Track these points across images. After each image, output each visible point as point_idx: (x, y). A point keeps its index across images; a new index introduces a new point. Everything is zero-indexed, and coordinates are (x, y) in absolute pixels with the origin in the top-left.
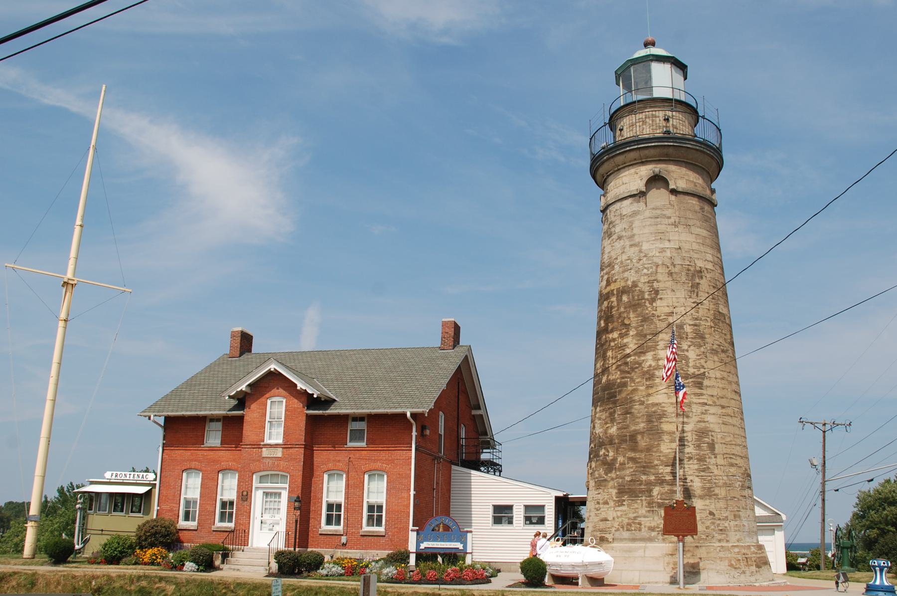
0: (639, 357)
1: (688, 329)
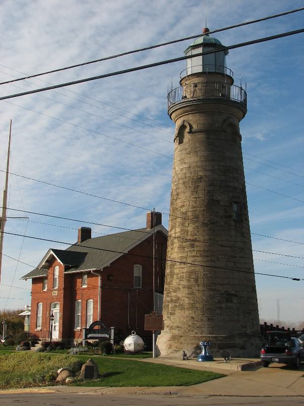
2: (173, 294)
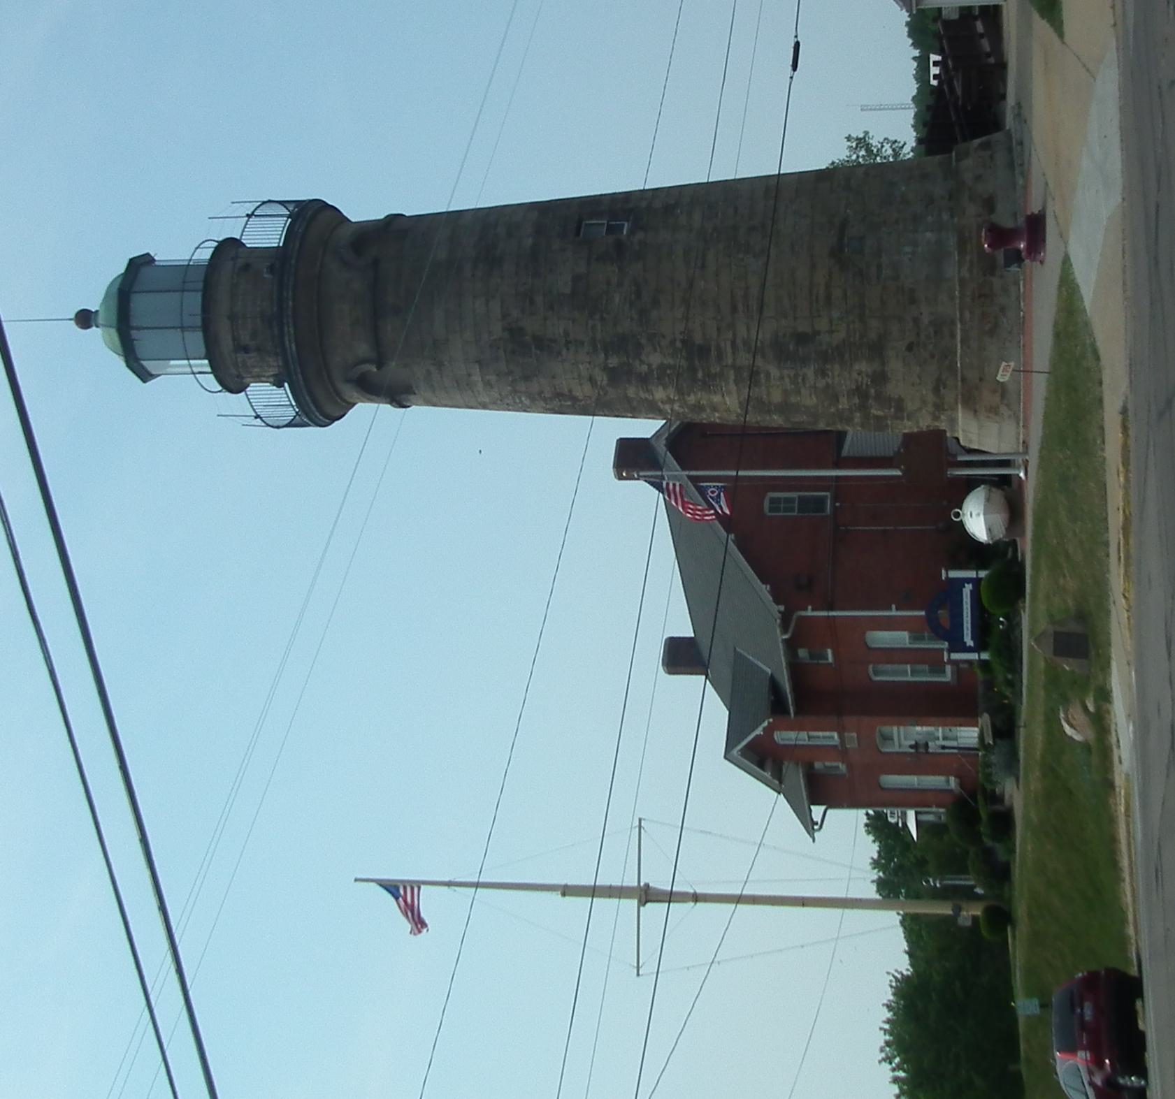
1: (614, 362)
2: (844, 403)
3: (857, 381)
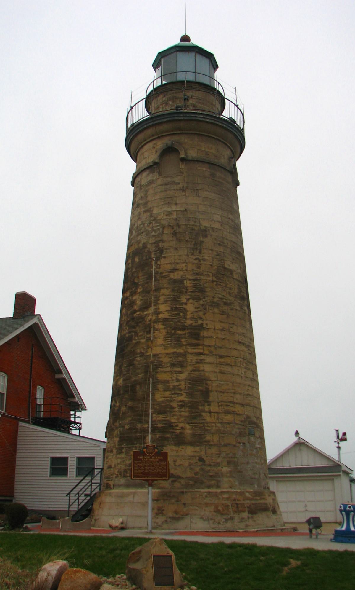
0: (143, 312)
3: (177, 426)
